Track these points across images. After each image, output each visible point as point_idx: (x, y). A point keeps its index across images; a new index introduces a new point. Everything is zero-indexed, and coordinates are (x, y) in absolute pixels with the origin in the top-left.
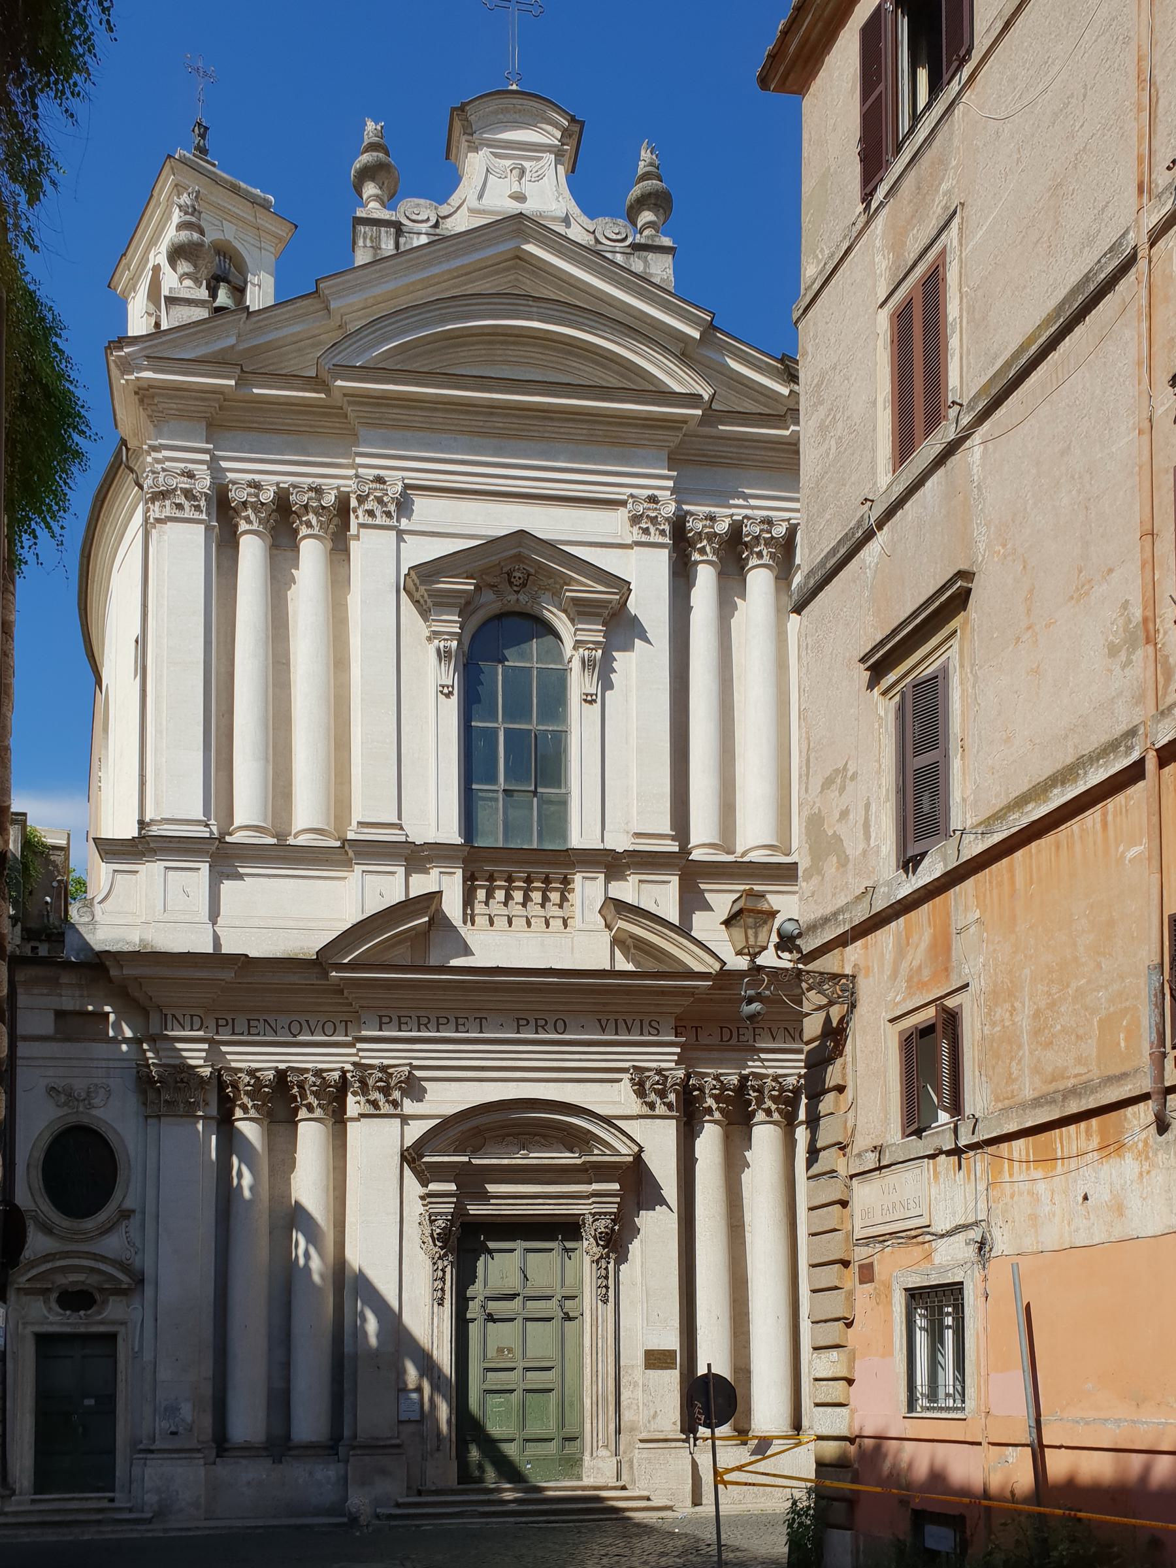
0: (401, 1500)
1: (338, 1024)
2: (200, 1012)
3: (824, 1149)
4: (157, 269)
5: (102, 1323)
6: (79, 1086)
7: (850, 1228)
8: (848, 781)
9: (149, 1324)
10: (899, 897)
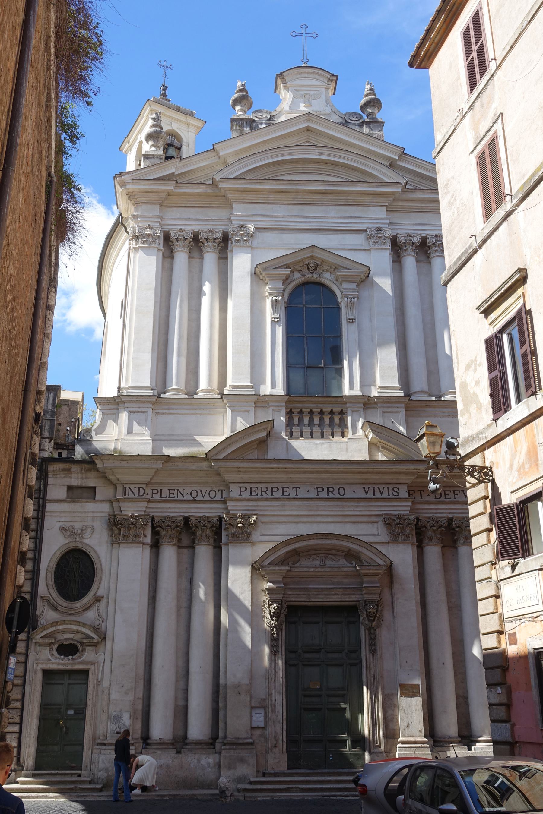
0: (252, 779)
1: (217, 492)
2: (144, 486)
3: (478, 567)
4: (141, 142)
5: (81, 663)
6: (78, 526)
7: (501, 611)
8: (477, 366)
9: (108, 663)
10: (508, 426)
